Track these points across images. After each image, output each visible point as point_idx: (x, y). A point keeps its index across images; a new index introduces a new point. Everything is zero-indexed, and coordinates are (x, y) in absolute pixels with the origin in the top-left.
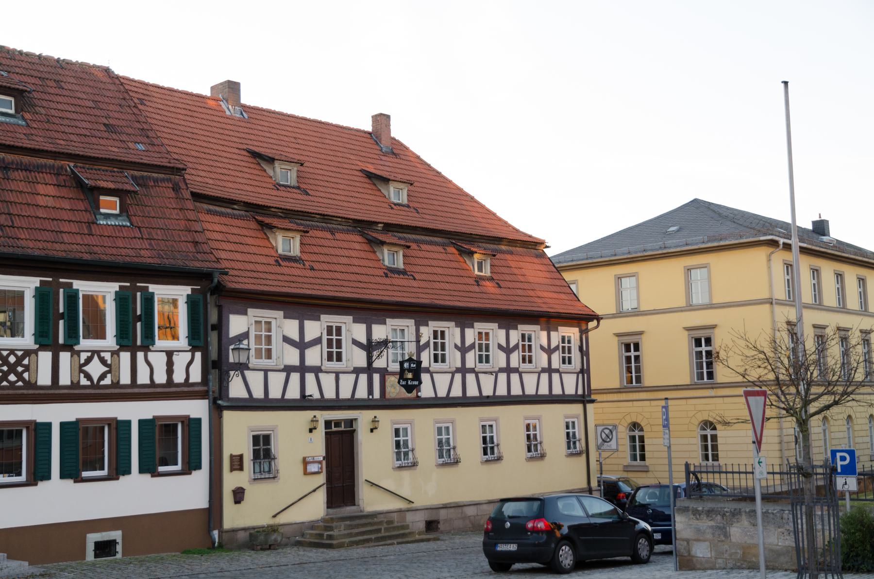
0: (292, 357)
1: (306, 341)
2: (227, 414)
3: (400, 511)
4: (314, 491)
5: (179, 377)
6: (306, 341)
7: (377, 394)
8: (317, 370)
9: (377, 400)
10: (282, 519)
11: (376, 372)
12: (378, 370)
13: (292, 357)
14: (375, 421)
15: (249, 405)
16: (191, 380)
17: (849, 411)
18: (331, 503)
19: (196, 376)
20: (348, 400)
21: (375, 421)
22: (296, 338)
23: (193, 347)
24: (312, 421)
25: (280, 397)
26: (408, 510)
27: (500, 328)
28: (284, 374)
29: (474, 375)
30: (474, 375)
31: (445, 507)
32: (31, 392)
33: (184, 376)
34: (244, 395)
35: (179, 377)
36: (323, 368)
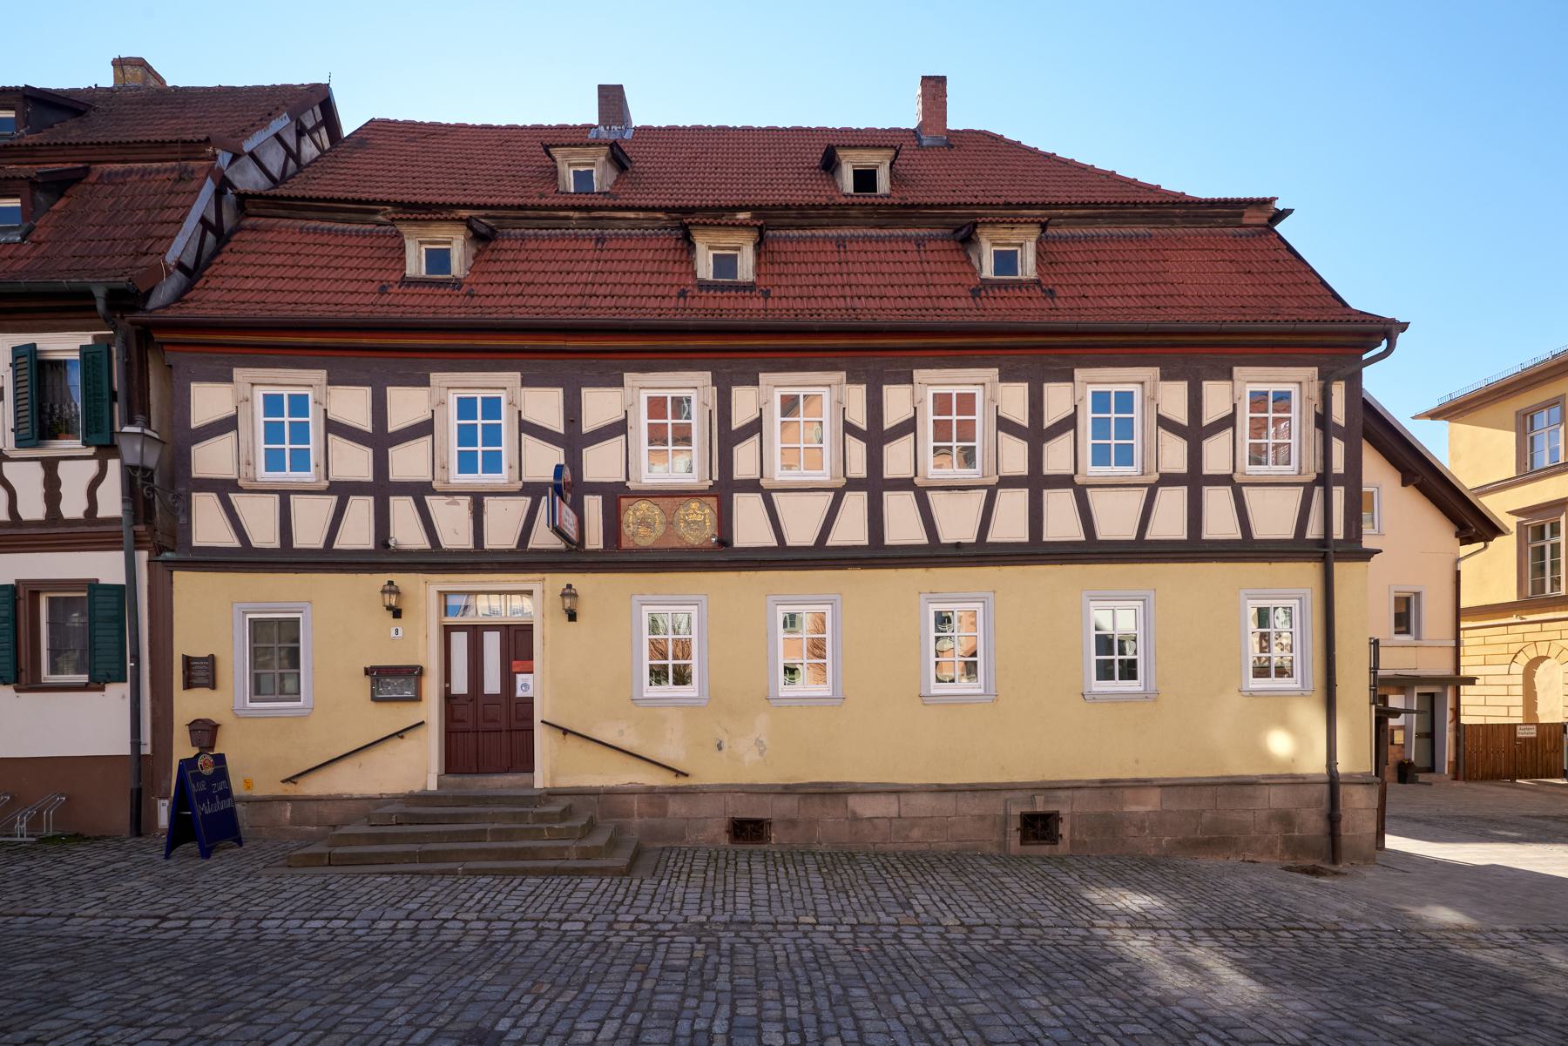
0: (354, 463)
1: (369, 429)
2: (181, 579)
3: (650, 791)
4: (400, 734)
5: (73, 506)
6: (369, 429)
7: (1338, 532)
8: (419, 491)
9: (595, 552)
10: (313, 787)
11: (594, 493)
12: (405, 488)
13: (354, 463)
14: (569, 593)
15: (243, 559)
16: (102, 513)
17: (1122, 620)
18: (453, 762)
19: (111, 503)
20: (511, 551)
21: (569, 593)
22: (366, 424)
23: (99, 447)
24: (563, 595)
25: (321, 546)
26: (675, 791)
27: (1004, 378)
28: (525, 502)
29: (908, 497)
30: (908, 497)
31: (787, 790)
32: (94, 529)
33: (84, 505)
34: (229, 540)
35: (73, 506)
36: (435, 485)
